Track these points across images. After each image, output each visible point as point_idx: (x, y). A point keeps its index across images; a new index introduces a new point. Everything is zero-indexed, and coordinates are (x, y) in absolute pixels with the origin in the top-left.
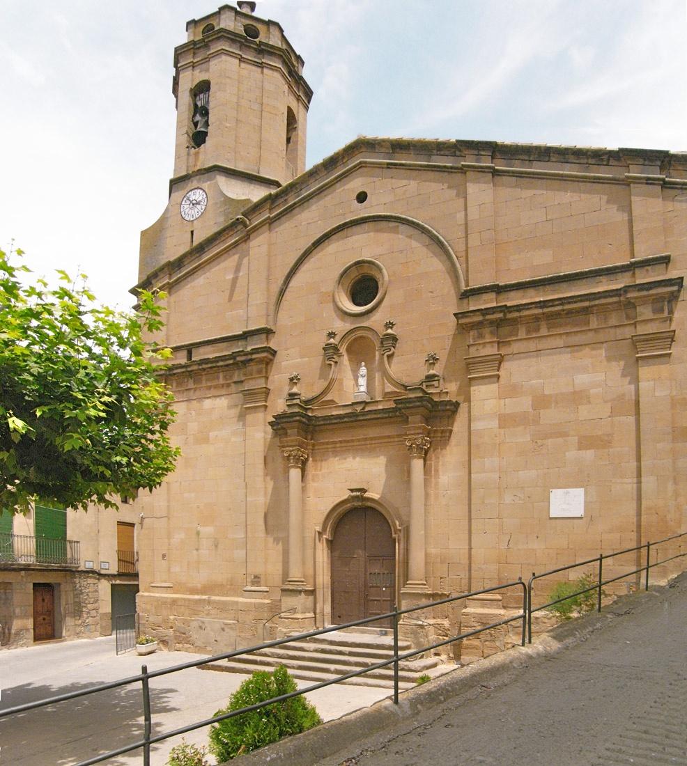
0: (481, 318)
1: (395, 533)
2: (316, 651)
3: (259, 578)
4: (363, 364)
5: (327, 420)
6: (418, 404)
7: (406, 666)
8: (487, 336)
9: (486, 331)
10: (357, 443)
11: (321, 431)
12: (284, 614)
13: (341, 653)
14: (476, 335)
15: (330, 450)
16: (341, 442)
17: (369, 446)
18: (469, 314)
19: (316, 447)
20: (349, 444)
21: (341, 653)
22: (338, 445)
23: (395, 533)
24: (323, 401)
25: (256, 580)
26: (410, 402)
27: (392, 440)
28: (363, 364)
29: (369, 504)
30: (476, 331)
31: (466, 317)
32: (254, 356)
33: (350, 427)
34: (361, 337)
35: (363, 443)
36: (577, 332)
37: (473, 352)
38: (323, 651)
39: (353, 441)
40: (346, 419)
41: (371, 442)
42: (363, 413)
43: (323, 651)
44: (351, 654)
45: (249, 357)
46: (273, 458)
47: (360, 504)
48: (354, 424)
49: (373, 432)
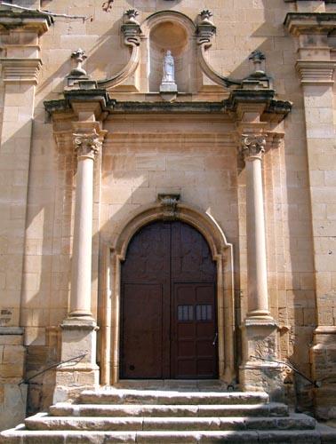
0: (315, 23)
1: (218, 253)
2: (141, 414)
3: (9, 313)
4: (169, 52)
5: (128, 107)
6: (262, 98)
7: (299, 421)
8: (318, 43)
9: (318, 37)
10: (166, 140)
11: (115, 120)
12: (66, 364)
13: (200, 413)
14: (307, 40)
15: (126, 145)
16: (143, 136)
17: (180, 144)
18: (305, 17)
19: (108, 140)
20: (155, 140)
21: (186, 413)
22: (140, 140)
23: (218, 253)
24: (120, 86)
25: (6, 316)
26: (253, 96)
27: (211, 140)
28: (169, 52)
29: (182, 216)
30: (306, 36)
31: (300, 19)
32: (26, 21)
33: (153, 120)
34: (169, 23)
35: (174, 140)
36: (134, 120)
37: (305, 56)
38: (156, 413)
39: (160, 136)
40: (154, 109)
41: (183, 140)
42: (179, 105)
43: (156, 413)
44: (200, 413)
45: (19, 20)
46: (43, 149)
47: (171, 214)
48: (164, 116)
49: (185, 128)
